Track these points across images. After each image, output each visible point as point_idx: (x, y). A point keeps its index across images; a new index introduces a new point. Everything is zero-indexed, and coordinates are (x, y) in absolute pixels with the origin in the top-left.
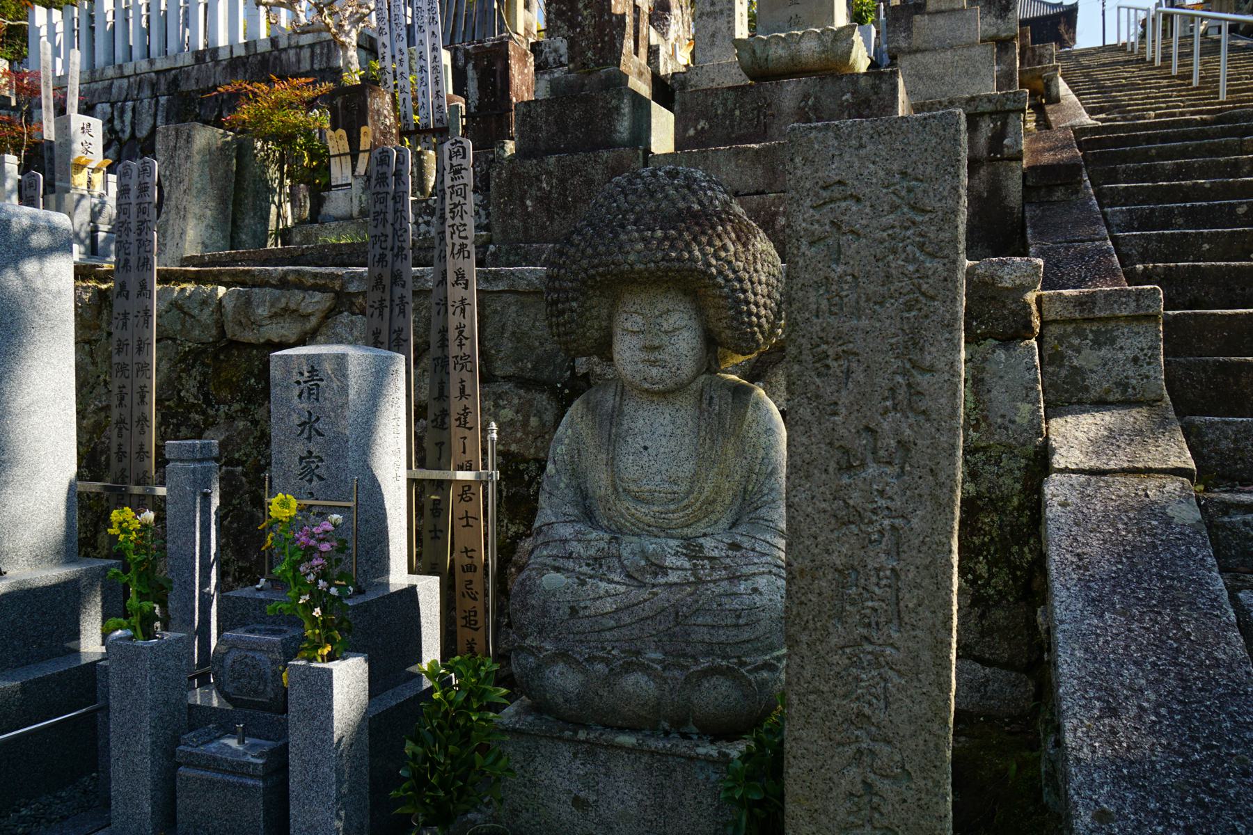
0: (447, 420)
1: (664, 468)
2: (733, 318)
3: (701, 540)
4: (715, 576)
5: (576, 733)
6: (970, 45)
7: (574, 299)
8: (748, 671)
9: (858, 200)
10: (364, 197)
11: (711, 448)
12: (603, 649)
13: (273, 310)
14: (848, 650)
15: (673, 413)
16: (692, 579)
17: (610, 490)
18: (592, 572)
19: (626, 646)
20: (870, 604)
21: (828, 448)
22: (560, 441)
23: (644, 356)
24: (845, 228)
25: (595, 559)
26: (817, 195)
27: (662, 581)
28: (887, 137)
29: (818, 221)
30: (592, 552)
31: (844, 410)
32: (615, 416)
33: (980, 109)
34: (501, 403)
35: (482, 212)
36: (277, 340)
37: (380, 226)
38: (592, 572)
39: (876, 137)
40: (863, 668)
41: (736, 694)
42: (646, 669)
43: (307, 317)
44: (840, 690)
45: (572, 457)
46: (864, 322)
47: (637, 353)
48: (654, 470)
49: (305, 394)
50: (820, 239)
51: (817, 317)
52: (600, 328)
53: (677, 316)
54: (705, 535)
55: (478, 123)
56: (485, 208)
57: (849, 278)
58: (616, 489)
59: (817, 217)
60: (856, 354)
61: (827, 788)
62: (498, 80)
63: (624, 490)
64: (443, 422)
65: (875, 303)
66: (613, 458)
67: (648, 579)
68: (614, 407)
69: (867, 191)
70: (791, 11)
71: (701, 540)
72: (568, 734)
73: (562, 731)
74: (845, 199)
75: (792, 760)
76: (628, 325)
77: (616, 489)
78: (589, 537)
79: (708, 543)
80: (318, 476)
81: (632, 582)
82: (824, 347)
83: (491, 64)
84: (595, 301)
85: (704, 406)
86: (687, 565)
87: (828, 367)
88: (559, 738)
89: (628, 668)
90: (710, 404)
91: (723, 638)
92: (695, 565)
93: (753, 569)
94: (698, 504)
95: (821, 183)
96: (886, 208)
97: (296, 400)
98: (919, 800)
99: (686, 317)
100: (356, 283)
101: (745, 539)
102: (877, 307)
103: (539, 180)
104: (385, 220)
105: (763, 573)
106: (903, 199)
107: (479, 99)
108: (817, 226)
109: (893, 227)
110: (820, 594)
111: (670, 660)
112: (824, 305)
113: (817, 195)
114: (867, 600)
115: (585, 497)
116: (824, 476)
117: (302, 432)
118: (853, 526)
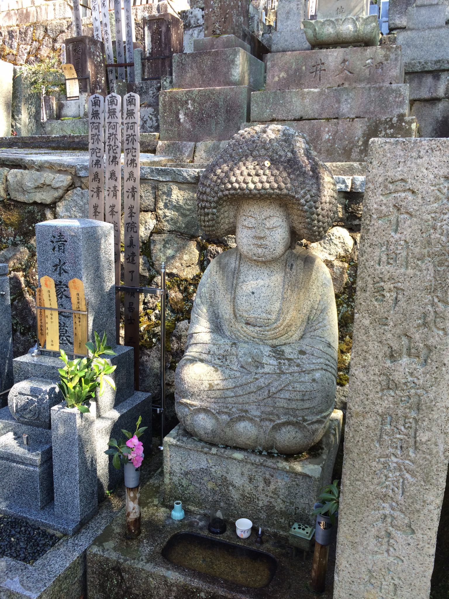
0: (135, 258)
1: (263, 305)
2: (309, 224)
3: (283, 348)
4: (291, 370)
5: (211, 449)
6: (440, 27)
7: (215, 208)
8: (309, 424)
9: (413, 192)
10: (86, 106)
11: (291, 295)
12: (227, 408)
13: (37, 184)
14: (382, 460)
15: (269, 273)
16: (278, 371)
17: (232, 316)
18: (221, 364)
19: (240, 407)
20: (398, 436)
21: (379, 344)
22: (204, 285)
23: (255, 241)
24: (403, 210)
25: (223, 356)
26: (386, 187)
27: (261, 371)
28: (438, 153)
29: (385, 204)
30: (221, 352)
31: (391, 323)
32: (236, 273)
33: (442, 68)
34: (167, 246)
35: (154, 119)
36: (39, 202)
37: (96, 143)
38: (221, 364)
39: (430, 151)
40: (391, 471)
41: (299, 435)
42: (251, 420)
43: (56, 189)
44: (376, 481)
45: (211, 295)
46: (410, 272)
47: (251, 239)
48: (257, 306)
49: (57, 249)
50: (385, 216)
51: (379, 265)
52: (229, 223)
53: (275, 219)
54: (285, 344)
55: (151, 64)
56: (156, 116)
57: (402, 243)
58: (235, 316)
59: (385, 201)
60: (403, 290)
61: (363, 532)
62: (163, 38)
63: (240, 316)
64: (133, 260)
65: (418, 259)
66: (234, 298)
67: (253, 369)
68: (235, 268)
69: (420, 187)
70: (338, 4)
71: (283, 348)
72: (206, 450)
73: (203, 448)
74: (404, 191)
75: (343, 514)
76: (246, 223)
77: (235, 316)
78: (219, 342)
79: (287, 350)
80: (65, 296)
81: (244, 370)
82: (382, 284)
83: (159, 27)
84: (226, 208)
85: (287, 270)
86: (275, 363)
87: (384, 296)
88: (201, 451)
89: (241, 419)
90: (291, 269)
91: (295, 406)
92: (280, 363)
93: (313, 367)
94: (282, 327)
95: (390, 179)
96: (432, 199)
97: (51, 252)
98: (418, 545)
99: (280, 220)
100: (84, 172)
101: (308, 348)
102: (419, 263)
103: (187, 103)
104: (98, 140)
105: (319, 369)
106: (444, 194)
107: (152, 48)
108: (384, 207)
109: (435, 212)
110: (367, 427)
111: (264, 416)
112: (384, 258)
113: (386, 187)
114: (396, 433)
115: (217, 317)
116: (375, 361)
117: (56, 270)
118: (391, 391)
